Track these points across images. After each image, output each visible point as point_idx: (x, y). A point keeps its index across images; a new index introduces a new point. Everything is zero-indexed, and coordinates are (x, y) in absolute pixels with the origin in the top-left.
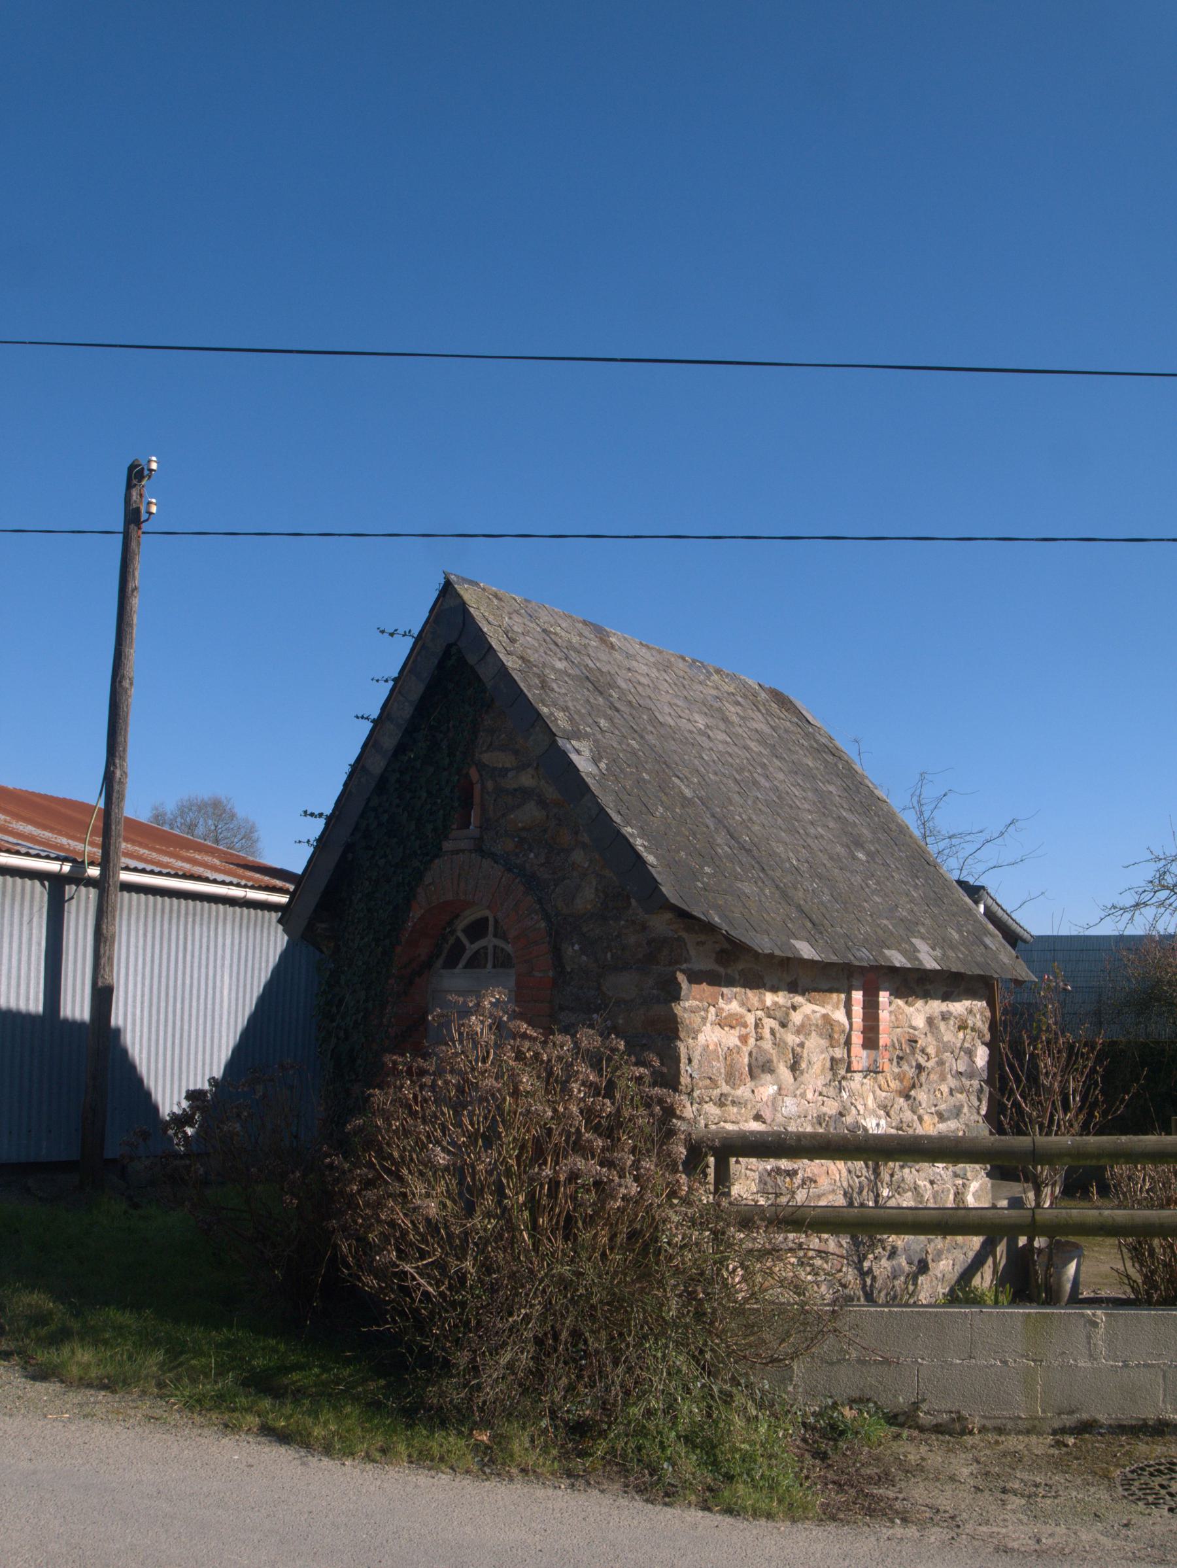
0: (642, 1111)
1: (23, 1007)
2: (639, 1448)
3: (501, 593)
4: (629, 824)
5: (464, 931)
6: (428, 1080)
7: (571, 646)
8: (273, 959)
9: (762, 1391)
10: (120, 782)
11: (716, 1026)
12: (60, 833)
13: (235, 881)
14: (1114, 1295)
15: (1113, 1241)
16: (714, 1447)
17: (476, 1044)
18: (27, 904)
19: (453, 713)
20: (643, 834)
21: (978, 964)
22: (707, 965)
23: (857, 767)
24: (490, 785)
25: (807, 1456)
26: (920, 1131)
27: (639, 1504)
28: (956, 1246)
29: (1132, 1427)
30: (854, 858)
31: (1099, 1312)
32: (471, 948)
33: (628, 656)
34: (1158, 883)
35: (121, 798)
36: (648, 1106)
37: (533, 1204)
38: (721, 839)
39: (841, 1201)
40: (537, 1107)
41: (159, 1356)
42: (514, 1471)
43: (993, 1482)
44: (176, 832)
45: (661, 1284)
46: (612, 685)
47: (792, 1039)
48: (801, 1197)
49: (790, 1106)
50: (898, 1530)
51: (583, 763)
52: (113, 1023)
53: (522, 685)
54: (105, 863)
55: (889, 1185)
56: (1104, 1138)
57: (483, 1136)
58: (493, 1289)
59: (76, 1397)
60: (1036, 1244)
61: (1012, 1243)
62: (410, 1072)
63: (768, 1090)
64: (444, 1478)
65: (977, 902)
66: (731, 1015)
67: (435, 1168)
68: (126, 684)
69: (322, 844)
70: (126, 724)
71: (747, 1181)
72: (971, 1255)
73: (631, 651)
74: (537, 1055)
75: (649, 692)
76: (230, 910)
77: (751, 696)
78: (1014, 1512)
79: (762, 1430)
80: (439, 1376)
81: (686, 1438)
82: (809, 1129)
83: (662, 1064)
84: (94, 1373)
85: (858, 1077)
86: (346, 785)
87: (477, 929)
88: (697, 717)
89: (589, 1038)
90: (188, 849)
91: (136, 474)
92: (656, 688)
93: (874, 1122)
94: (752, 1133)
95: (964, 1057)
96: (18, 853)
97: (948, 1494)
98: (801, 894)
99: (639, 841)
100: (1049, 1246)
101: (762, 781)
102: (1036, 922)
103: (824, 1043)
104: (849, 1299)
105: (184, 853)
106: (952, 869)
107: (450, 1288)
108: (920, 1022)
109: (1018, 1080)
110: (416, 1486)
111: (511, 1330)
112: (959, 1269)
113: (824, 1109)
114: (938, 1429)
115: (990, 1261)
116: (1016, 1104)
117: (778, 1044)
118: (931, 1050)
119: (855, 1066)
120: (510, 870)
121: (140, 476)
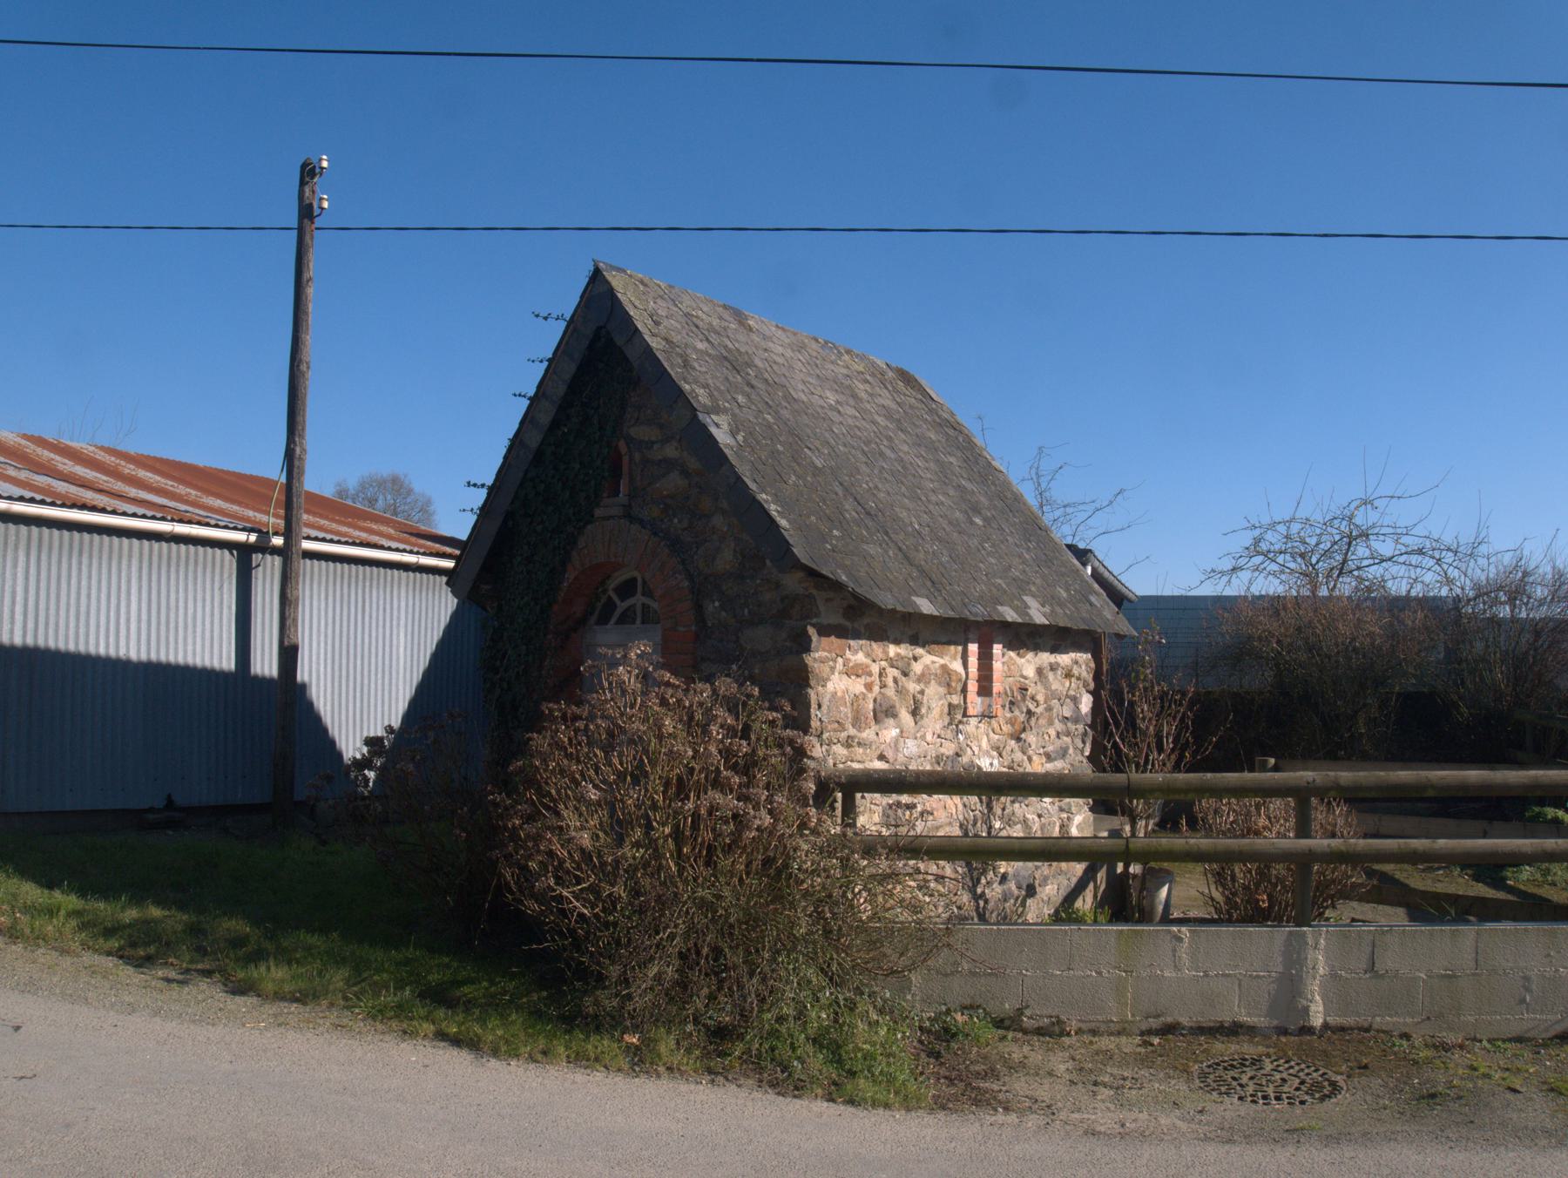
0: (776, 751)
1: (216, 665)
2: (773, 1049)
3: (646, 280)
4: (763, 491)
5: (616, 590)
6: (580, 724)
7: (712, 329)
8: (444, 619)
9: (885, 1001)
10: (300, 459)
11: (844, 674)
12: (247, 506)
13: (408, 548)
14: (1201, 915)
15: (1199, 868)
16: (839, 1047)
17: (624, 692)
18: (217, 571)
19: (602, 387)
20: (777, 499)
21: (1083, 619)
22: (835, 619)
23: (979, 441)
24: (637, 456)
25: (923, 1055)
26: (1029, 769)
27: (771, 1096)
28: (1061, 872)
29: (1211, 1029)
30: (972, 523)
31: (1183, 929)
32: (621, 606)
33: (765, 338)
34: (1255, 549)
35: (301, 472)
36: (780, 746)
37: (677, 835)
38: (848, 505)
39: (957, 832)
40: (678, 747)
41: (344, 973)
42: (661, 1069)
43: (1086, 1077)
44: (359, 506)
45: (793, 906)
46: (750, 364)
47: (913, 687)
48: (920, 827)
49: (911, 747)
50: (1000, 1117)
51: (722, 436)
52: (299, 678)
53: (666, 364)
54: (288, 533)
55: (1001, 819)
56: (1192, 775)
57: (632, 775)
58: (641, 911)
59: (271, 1009)
60: (1131, 870)
61: (1112, 869)
62: (564, 718)
63: (890, 733)
64: (599, 1076)
65: (1084, 565)
66: (857, 665)
67: (589, 803)
68: (303, 367)
69: (485, 511)
70: (304, 404)
71: (872, 814)
72: (1074, 880)
73: (767, 333)
74: (679, 701)
75: (784, 370)
76: (404, 574)
77: (878, 374)
78: (1103, 1101)
79: (883, 1032)
80: (595, 988)
81: (814, 1040)
82: (928, 768)
83: (793, 708)
84: (287, 988)
85: (973, 721)
86: (506, 458)
87: (627, 589)
88: (828, 394)
89: (726, 686)
90: (365, 520)
91: (308, 172)
92: (791, 367)
93: (988, 761)
94: (876, 771)
95: (1069, 704)
96: (208, 525)
97: (1046, 1087)
98: (921, 555)
99: (773, 507)
100: (1144, 874)
101: (888, 452)
102: (1140, 584)
103: (942, 690)
104: (963, 919)
105: (361, 523)
106: (1064, 534)
107: (604, 910)
108: (1030, 672)
109: (1117, 725)
110: (574, 1082)
111: (658, 946)
112: (1063, 893)
113: (942, 750)
114: (1040, 1032)
115: (1091, 886)
116: (1115, 745)
117: (900, 691)
118: (1040, 698)
119: (971, 711)
120: (655, 534)
121: (312, 173)
